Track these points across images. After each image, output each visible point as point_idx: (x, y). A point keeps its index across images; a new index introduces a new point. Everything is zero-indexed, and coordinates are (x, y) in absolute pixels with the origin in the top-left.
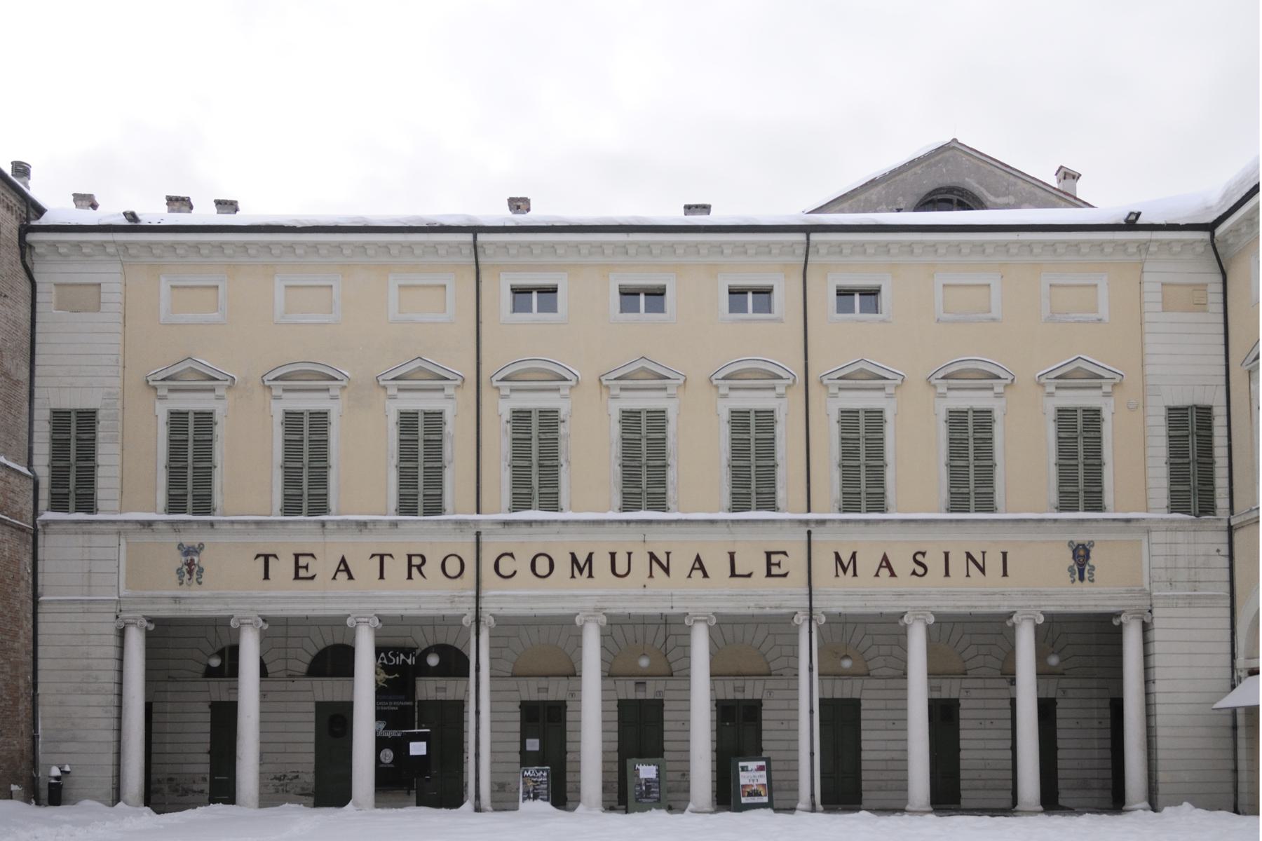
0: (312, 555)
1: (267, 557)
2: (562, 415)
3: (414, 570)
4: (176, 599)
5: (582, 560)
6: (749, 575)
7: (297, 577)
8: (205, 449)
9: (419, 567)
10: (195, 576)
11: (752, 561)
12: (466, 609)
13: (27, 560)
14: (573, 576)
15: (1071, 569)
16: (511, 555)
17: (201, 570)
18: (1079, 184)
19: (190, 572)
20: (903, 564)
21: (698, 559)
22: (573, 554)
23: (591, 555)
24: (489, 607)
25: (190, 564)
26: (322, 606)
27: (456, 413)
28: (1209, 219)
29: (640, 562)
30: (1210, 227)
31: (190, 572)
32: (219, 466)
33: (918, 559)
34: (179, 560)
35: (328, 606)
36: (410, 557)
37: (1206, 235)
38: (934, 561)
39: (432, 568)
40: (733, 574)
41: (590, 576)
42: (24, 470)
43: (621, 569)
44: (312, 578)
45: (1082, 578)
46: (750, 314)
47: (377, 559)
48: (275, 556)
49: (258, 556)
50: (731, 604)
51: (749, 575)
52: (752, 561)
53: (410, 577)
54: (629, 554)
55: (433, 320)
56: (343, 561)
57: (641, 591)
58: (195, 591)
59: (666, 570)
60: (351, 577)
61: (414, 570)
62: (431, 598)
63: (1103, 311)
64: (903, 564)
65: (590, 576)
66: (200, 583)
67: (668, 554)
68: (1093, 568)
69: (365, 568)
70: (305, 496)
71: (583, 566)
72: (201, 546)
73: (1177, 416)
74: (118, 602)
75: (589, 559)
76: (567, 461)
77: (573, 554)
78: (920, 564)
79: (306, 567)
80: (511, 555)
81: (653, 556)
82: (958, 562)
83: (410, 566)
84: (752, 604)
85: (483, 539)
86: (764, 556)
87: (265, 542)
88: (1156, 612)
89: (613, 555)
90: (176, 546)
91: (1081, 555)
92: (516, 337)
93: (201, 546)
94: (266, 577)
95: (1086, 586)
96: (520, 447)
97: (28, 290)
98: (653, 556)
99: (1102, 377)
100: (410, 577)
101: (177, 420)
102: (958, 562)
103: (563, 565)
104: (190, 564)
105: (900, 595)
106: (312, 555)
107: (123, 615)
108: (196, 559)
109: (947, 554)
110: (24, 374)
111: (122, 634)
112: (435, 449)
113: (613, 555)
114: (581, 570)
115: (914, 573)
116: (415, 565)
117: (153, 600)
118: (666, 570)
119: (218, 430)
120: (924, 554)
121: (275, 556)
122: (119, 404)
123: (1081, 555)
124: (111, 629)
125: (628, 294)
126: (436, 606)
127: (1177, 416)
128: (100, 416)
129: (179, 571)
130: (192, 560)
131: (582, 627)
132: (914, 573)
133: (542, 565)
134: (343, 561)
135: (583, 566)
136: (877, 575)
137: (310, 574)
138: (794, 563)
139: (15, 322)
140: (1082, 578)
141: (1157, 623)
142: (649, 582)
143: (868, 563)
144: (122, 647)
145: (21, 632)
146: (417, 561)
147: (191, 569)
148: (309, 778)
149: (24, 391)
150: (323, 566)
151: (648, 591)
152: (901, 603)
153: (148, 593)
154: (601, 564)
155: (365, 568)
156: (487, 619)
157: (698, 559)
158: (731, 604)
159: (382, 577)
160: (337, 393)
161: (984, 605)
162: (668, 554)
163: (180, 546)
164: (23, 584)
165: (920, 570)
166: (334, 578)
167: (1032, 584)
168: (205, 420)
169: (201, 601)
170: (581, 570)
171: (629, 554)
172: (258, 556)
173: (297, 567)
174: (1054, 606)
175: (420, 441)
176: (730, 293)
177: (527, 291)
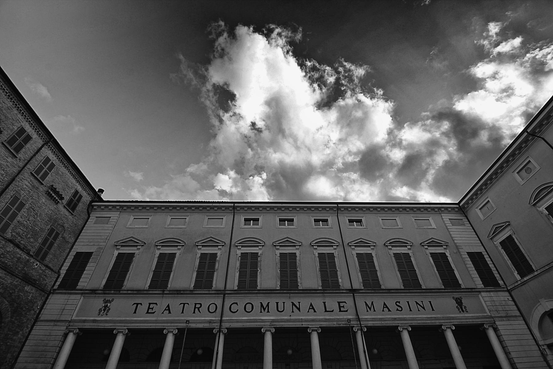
0: (345, 302)
3: (196, 309)
4: (94, 321)
6: (332, 311)
9: (198, 308)
13: (40, 303)
16: (237, 303)
18: (494, 98)
19: (104, 310)
22: (261, 303)
23: (268, 303)
24: (225, 325)
25: (106, 307)
27: (337, 253)
31: (104, 310)
36: (196, 304)
40: (326, 311)
41: (268, 312)
42: (55, 287)
49: (134, 304)
57: (289, 318)
61: (196, 309)
63: (434, 226)
65: (268, 312)
66: (107, 315)
68: (465, 307)
73: (471, 255)
74: (70, 322)
75: (268, 305)
77: (261, 303)
79: (152, 309)
83: (195, 308)
97: (86, 218)
108: (109, 305)
110: (72, 240)
111: (66, 336)
114: (264, 309)
115: (397, 310)
116: (197, 308)
120: (399, 302)
131: (264, 333)
132: (397, 310)
139: (76, 224)
140: (463, 311)
144: (63, 342)
145: (21, 332)
146: (198, 306)
148: (198, 186)
149: (70, 245)
151: (292, 318)
153: (84, 318)
164: (32, 312)
165: (400, 309)
170: (264, 309)
173: (149, 308)
176: (315, 221)
177: (249, 220)
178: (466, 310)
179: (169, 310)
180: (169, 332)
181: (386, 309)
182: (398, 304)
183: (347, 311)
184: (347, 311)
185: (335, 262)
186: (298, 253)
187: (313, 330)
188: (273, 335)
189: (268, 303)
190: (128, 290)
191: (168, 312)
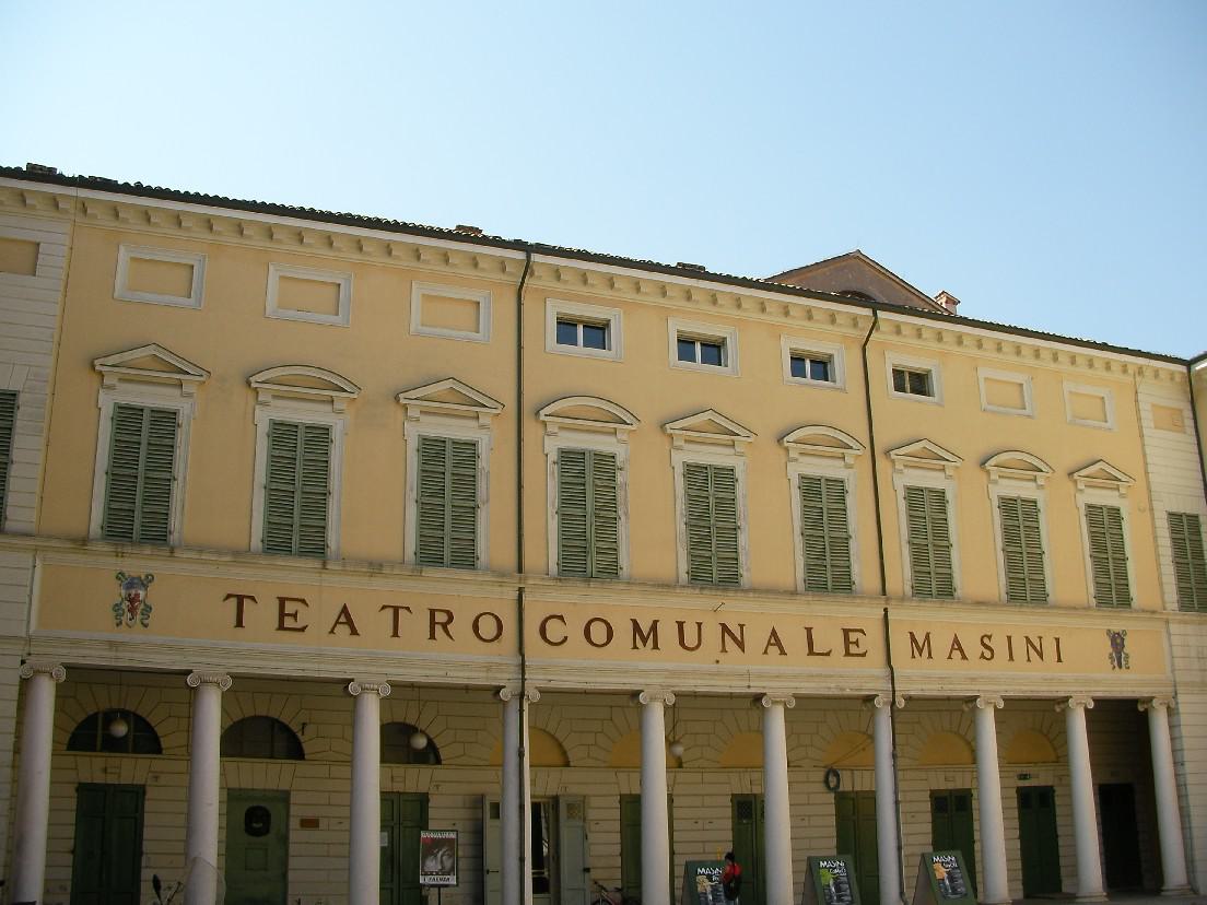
0: (303, 601)
1: (240, 599)
2: (619, 461)
4: (112, 645)
5: (645, 627)
6: (828, 654)
7: (281, 627)
8: (164, 453)
9: (444, 626)
10: (139, 617)
11: (828, 638)
12: (506, 678)
14: (635, 647)
15: (1111, 657)
16: (561, 618)
17: (148, 609)
19: (132, 610)
20: (972, 646)
21: (774, 633)
23: (655, 622)
24: (535, 680)
26: (316, 666)
27: (491, 440)
28: (1188, 357)
29: (712, 634)
30: (1189, 364)
31: (132, 610)
32: (180, 479)
33: (985, 640)
34: (118, 593)
35: (322, 666)
36: (432, 612)
37: (1183, 369)
38: (999, 644)
39: (461, 627)
40: (811, 652)
41: (656, 646)
43: (690, 640)
44: (303, 629)
45: (1120, 667)
46: (808, 379)
47: (390, 612)
48: (253, 598)
50: (813, 685)
51: (828, 654)
52: (828, 638)
53: (432, 636)
54: (699, 625)
55: (465, 336)
56: (345, 610)
58: (135, 635)
59: (741, 645)
60: (354, 632)
61: (438, 629)
62: (462, 660)
64: (972, 646)
66: (146, 626)
67: (742, 626)
68: (1127, 656)
69: (374, 624)
70: (296, 527)
71: (645, 635)
72: (150, 578)
73: (1175, 519)
76: (626, 514)
78: (988, 652)
79: (295, 616)
80: (561, 618)
81: (725, 628)
82: (1020, 648)
84: (832, 685)
85: (526, 599)
86: (841, 634)
87: (244, 578)
88: (1181, 698)
89: (681, 625)
90: (114, 574)
91: (1117, 641)
92: (561, 367)
93: (150, 578)
94: (239, 623)
95: (1122, 674)
96: (571, 496)
98: (725, 628)
99: (1120, 480)
100: (432, 636)
101: (127, 417)
102: (1020, 648)
103: (623, 632)
104: (132, 600)
105: (973, 679)
106: (303, 601)
107: (31, 661)
108: (142, 593)
109: (1009, 638)
111: (25, 685)
112: (467, 483)
113: (681, 625)
114: (644, 640)
116: (440, 622)
117: (75, 643)
118: (741, 645)
119: (181, 435)
120: (989, 637)
121: (253, 598)
122: (49, 390)
123: (1117, 641)
124: (14, 678)
125: (686, 344)
126: (467, 674)
127: (1175, 519)
128: (22, 399)
129: (117, 607)
130: (137, 595)
132: (983, 656)
133: (598, 633)
134: (345, 610)
135: (645, 635)
136: (950, 658)
137: (299, 625)
138: (872, 641)
140: (1120, 667)
141: (1182, 708)
142: (722, 657)
143: (941, 644)
147: (133, 603)
150: (318, 616)
152: (973, 687)
154: (667, 633)
155: (374, 624)
156: (532, 694)
157: (774, 633)
158: (813, 685)
159: (395, 634)
160: (343, 406)
161: (1044, 690)
162: (742, 626)
163: (120, 576)
165: (988, 654)
166: (332, 632)
167: (1082, 672)
168: (166, 420)
169: (147, 648)
170: (644, 640)
171: (699, 625)
172: (229, 596)
173: (282, 615)
174: (1104, 691)
175: (447, 475)
178: (1127, 662)
179: (778, 643)
180: (653, 699)
181: (774, 650)
182: (986, 641)
183: (864, 655)
184: (864, 655)
185: (1201, 541)
186: (338, 426)
187: (775, 703)
188: (385, 703)
189: (655, 622)
190: (50, 537)
191: (346, 629)
